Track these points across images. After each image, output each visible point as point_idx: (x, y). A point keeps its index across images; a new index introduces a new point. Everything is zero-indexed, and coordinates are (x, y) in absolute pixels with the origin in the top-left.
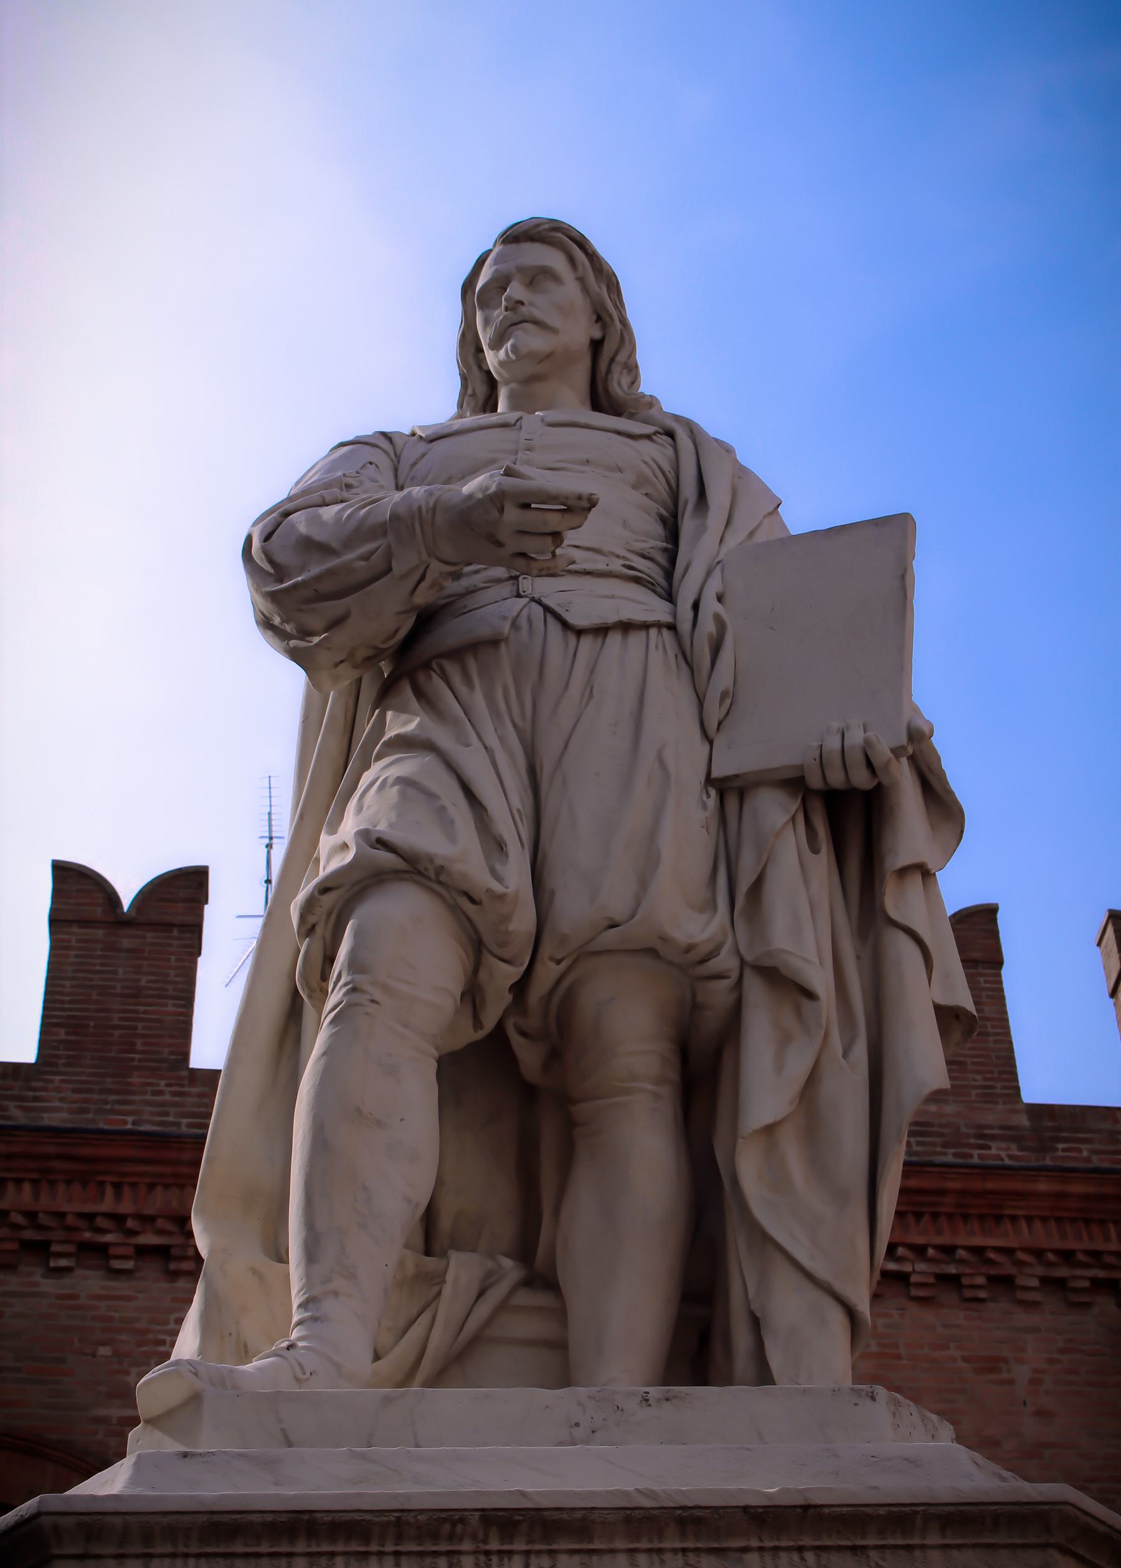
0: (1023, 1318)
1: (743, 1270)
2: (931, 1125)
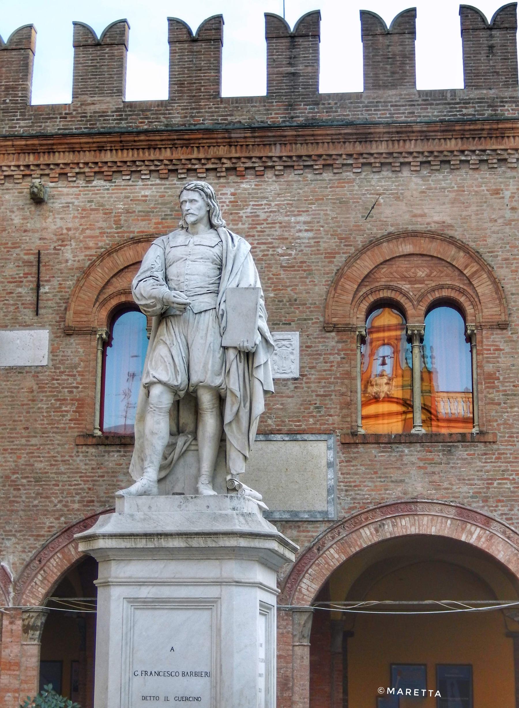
2: (484, 99)
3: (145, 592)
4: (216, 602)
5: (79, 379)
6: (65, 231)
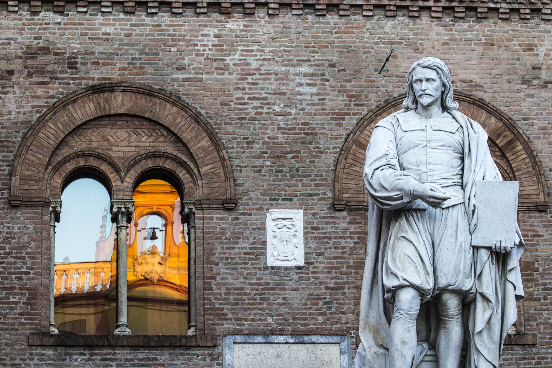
1: (474, 356)
5: (29, 262)
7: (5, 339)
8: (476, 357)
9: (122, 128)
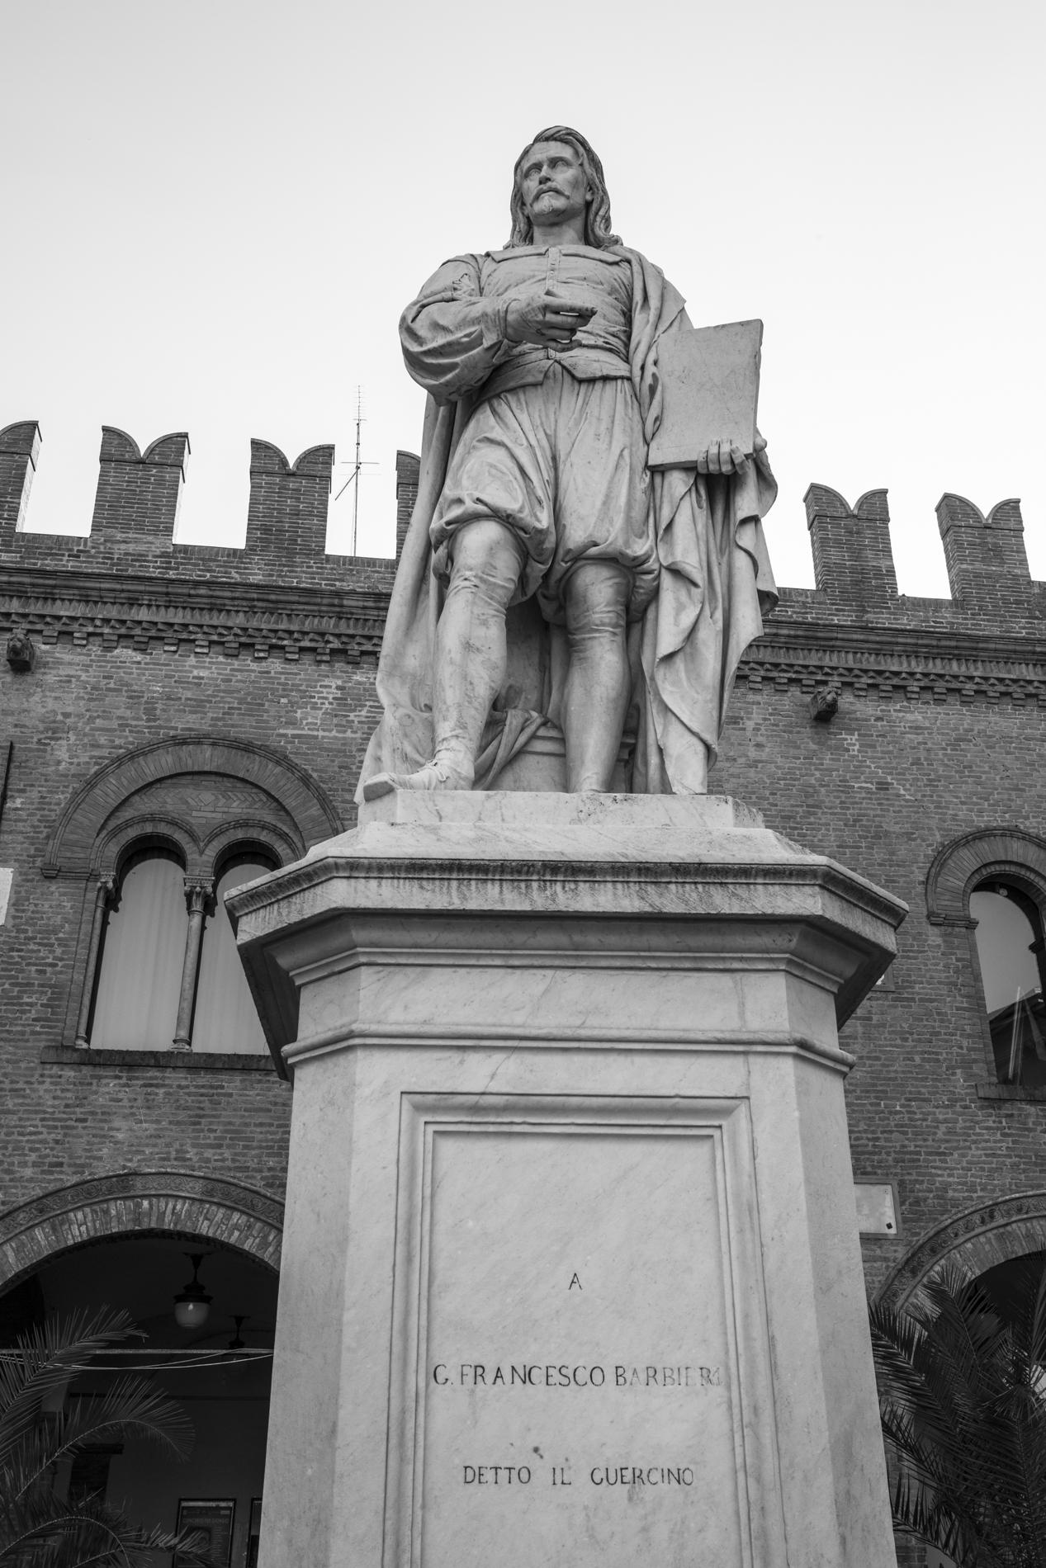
0: (751, 697)
1: (655, 725)
3: (478, 1074)
4: (726, 1112)
5: (59, 951)
6: (60, 717)
7: (7, 1053)
8: (659, 730)
9: (207, 788)
